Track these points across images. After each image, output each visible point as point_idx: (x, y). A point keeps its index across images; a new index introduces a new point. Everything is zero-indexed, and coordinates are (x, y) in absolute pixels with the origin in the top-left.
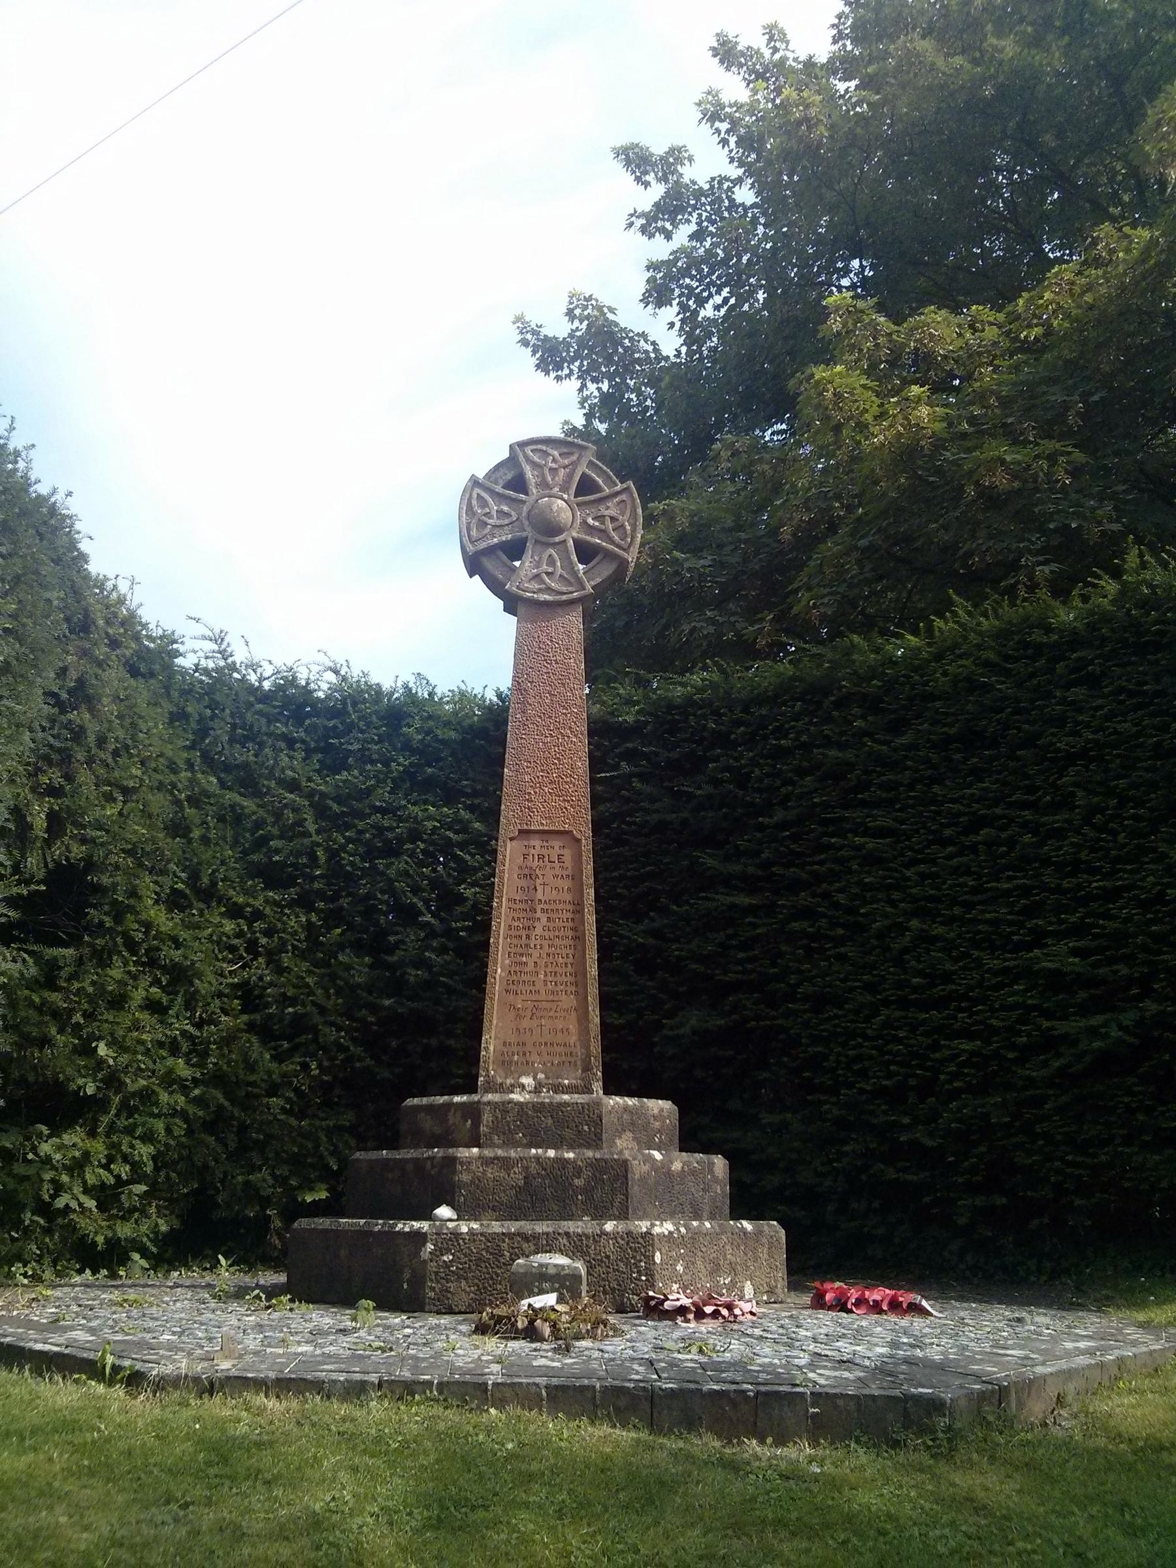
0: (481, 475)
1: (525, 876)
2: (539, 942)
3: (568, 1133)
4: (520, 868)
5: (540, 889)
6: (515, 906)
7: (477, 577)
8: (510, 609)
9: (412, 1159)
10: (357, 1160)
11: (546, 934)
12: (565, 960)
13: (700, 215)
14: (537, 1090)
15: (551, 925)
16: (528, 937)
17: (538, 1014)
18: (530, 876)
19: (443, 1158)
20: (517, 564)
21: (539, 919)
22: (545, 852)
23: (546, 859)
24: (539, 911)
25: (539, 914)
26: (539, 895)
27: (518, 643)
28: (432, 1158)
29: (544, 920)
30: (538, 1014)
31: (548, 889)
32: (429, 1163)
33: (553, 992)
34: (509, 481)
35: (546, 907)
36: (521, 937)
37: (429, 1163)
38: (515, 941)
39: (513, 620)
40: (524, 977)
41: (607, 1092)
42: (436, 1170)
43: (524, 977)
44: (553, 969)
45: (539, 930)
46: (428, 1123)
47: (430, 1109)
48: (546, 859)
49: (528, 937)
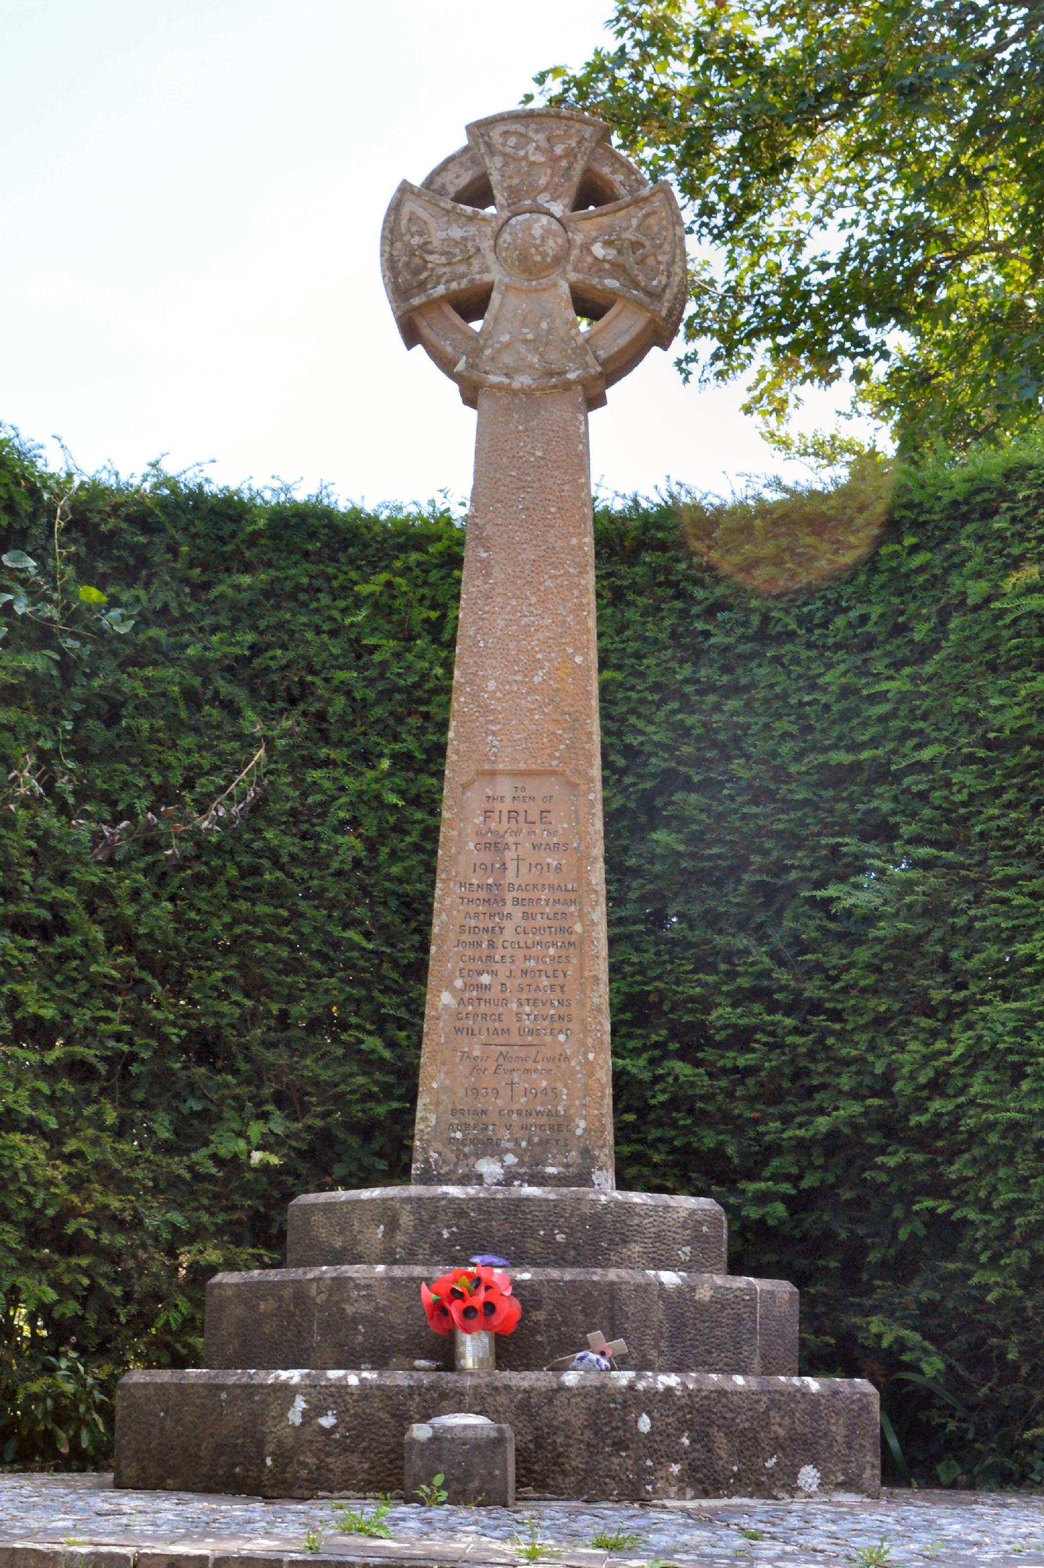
0: (417, 180)
1: (488, 846)
2: (508, 952)
3: (531, 1246)
4: (479, 833)
5: (511, 866)
6: (472, 896)
7: (419, 349)
8: (470, 399)
9: (293, 1281)
10: (220, 1285)
11: (522, 938)
12: (552, 981)
13: (345, 611)
14: (507, 1181)
15: (529, 924)
16: (491, 944)
17: (508, 1066)
18: (496, 846)
19: (333, 1279)
20: (477, 325)
21: (509, 916)
22: (521, 806)
23: (521, 818)
24: (509, 902)
25: (509, 908)
26: (510, 876)
27: (476, 471)
28: (318, 1280)
29: (517, 913)
30: (508, 1066)
31: (524, 868)
32: (314, 1286)
33: (531, 1032)
34: (465, 189)
35: (520, 895)
36: (479, 944)
37: (314, 1286)
38: (469, 952)
39: (471, 415)
40: (483, 1008)
41: (623, 1183)
42: (323, 1296)
43: (483, 1008)
44: (532, 995)
45: (508, 934)
46: (323, 1231)
47: (329, 1208)
48: (521, 818)
49: (491, 944)
